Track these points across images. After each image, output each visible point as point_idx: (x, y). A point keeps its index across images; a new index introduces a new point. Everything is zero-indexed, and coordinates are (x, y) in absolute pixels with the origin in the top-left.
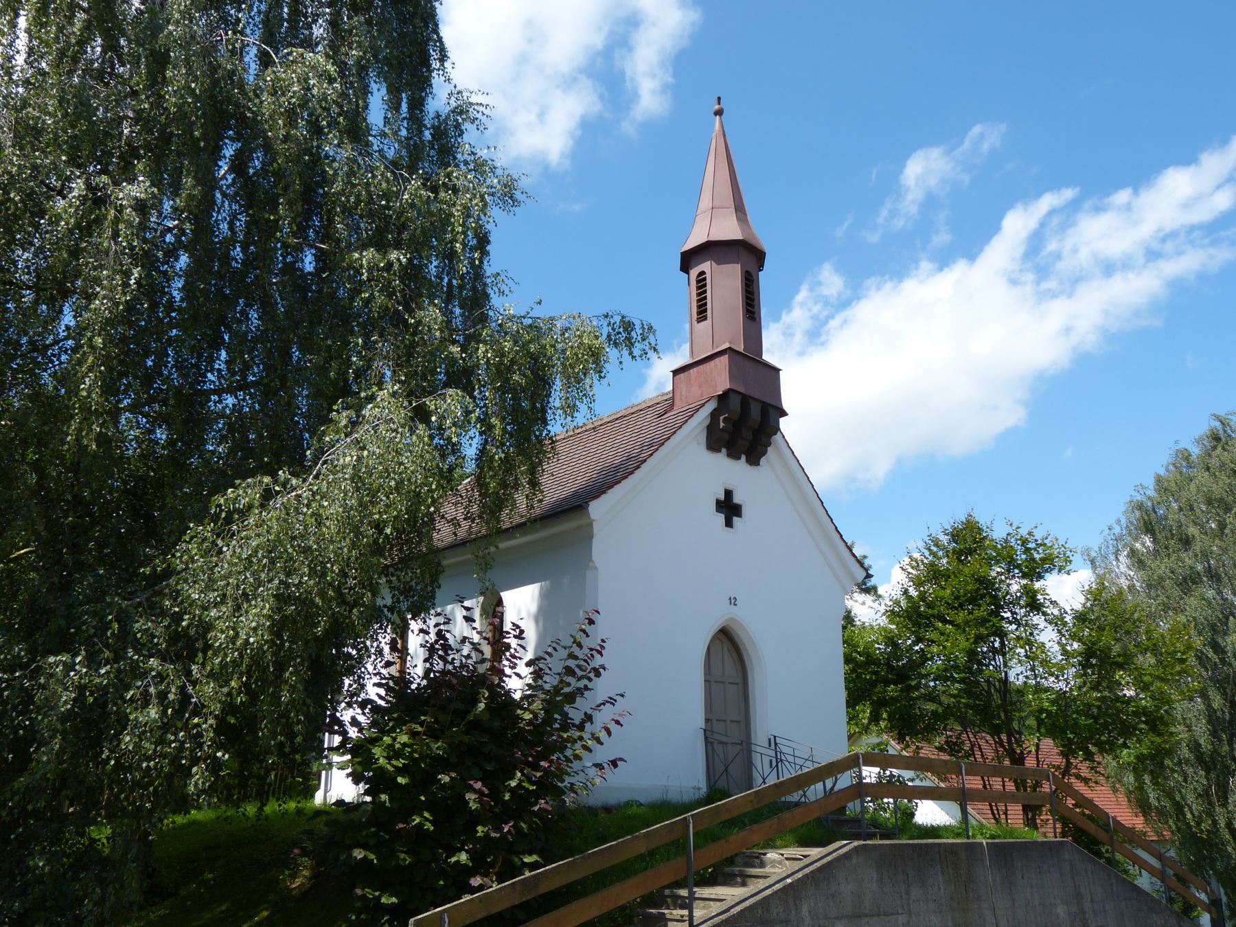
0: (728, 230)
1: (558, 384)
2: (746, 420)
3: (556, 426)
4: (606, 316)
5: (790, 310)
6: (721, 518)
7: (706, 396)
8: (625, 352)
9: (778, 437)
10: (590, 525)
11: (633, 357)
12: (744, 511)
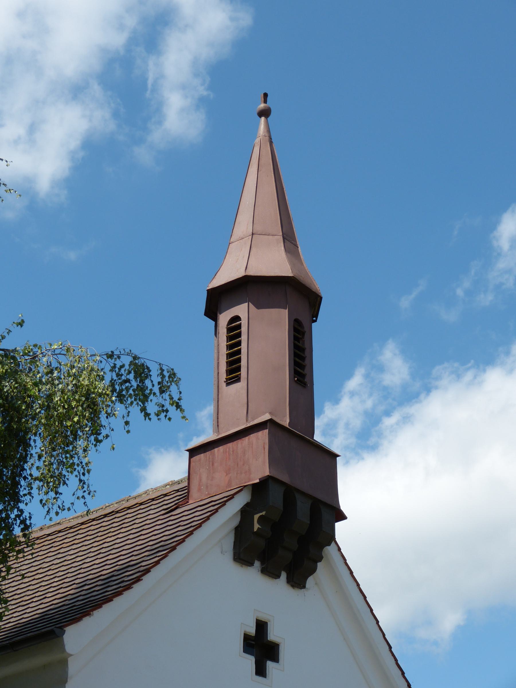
0: (273, 262)
1: (37, 445)
2: (289, 524)
3: (35, 510)
4: (111, 356)
5: (337, 401)
6: (250, 661)
7: (236, 485)
8: (135, 410)
9: (330, 549)
10: (64, 663)
11: (147, 415)
12: (284, 653)
